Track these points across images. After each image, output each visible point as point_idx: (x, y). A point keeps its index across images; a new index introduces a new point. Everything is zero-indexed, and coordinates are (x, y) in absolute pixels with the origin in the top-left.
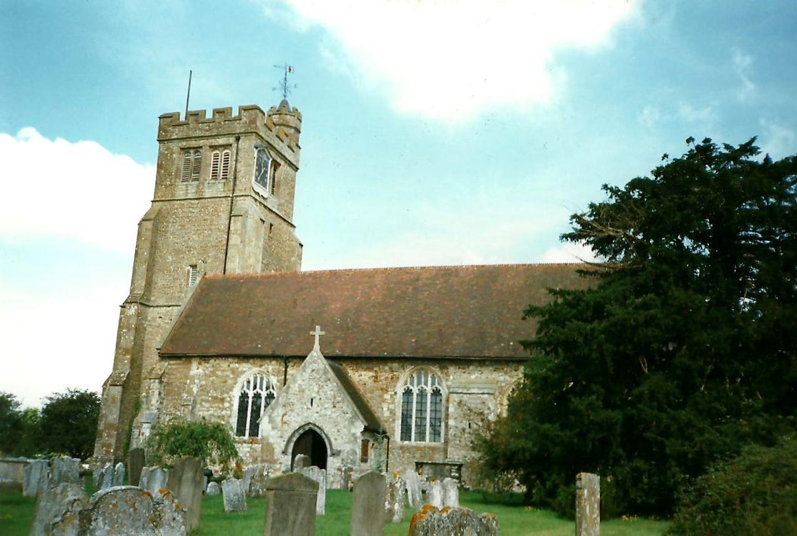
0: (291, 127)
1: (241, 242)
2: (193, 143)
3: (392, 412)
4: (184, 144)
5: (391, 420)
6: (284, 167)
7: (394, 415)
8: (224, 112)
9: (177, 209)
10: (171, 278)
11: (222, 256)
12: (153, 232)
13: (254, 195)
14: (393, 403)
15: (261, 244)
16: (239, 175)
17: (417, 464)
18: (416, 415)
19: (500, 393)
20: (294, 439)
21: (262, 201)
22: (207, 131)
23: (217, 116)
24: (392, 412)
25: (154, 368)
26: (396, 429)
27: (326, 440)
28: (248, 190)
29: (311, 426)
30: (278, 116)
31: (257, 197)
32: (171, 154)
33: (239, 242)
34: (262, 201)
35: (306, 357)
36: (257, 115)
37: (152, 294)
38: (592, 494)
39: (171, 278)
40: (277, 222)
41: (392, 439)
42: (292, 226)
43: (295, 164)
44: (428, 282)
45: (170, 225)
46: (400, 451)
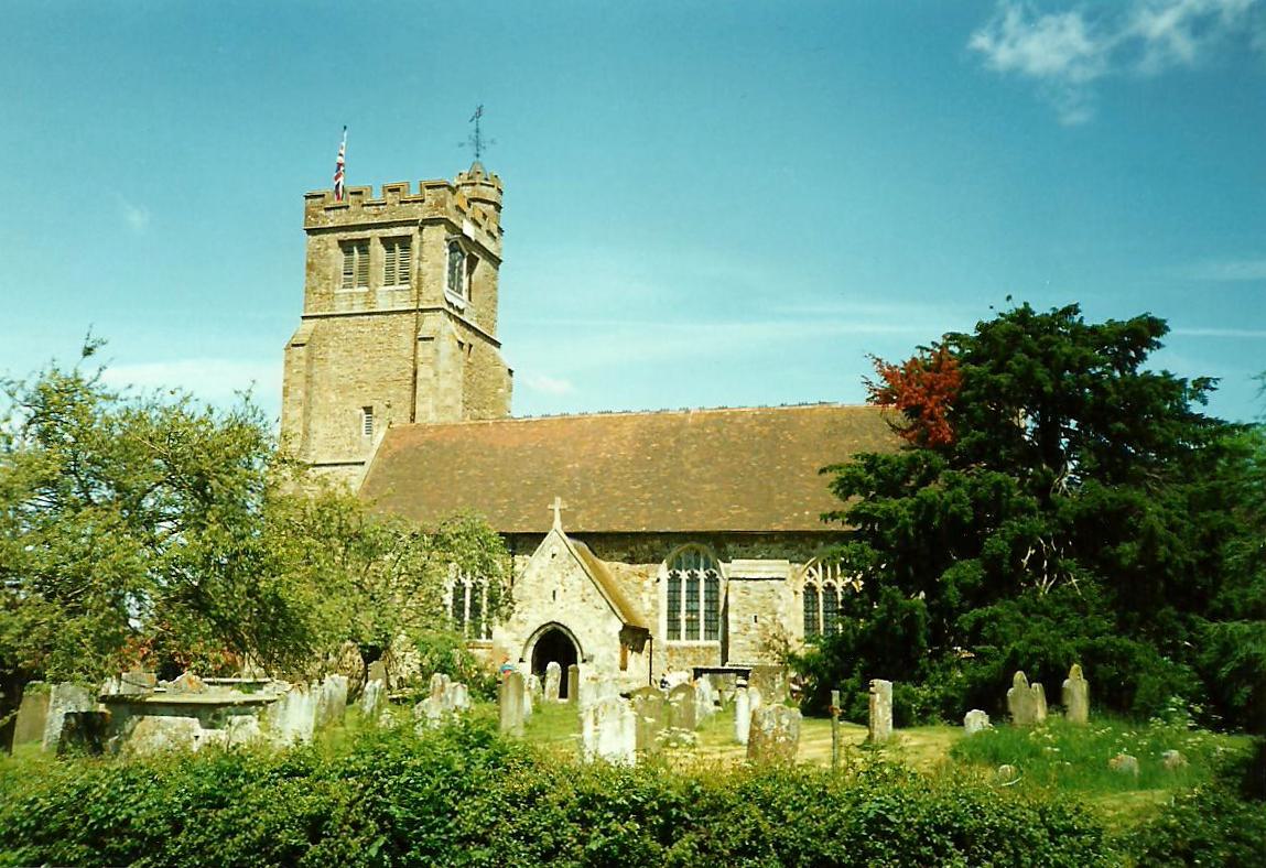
0: (489, 202)
1: (435, 375)
2: (357, 235)
3: (655, 604)
4: (343, 235)
5: (653, 614)
6: (482, 264)
7: (658, 607)
8: (398, 190)
9: (338, 327)
10: (337, 425)
11: (407, 394)
12: (308, 361)
13: (446, 307)
14: (655, 592)
15: (460, 376)
16: (426, 279)
17: (696, 670)
18: (680, 596)
19: (793, 577)
20: (534, 642)
21: (456, 314)
22: (376, 215)
23: (390, 194)
24: (655, 604)
25: (62, 471)
26: (661, 625)
27: (575, 643)
28: (439, 301)
29: (554, 625)
30: (470, 187)
31: (451, 310)
32: (326, 249)
33: (431, 375)
34: (456, 314)
35: (545, 534)
36: (445, 194)
37: (312, 448)
38: (884, 698)
39: (337, 425)
40: (477, 341)
41: (655, 638)
42: (497, 344)
43: (497, 254)
44: (694, 431)
45: (330, 351)
46: (667, 654)
